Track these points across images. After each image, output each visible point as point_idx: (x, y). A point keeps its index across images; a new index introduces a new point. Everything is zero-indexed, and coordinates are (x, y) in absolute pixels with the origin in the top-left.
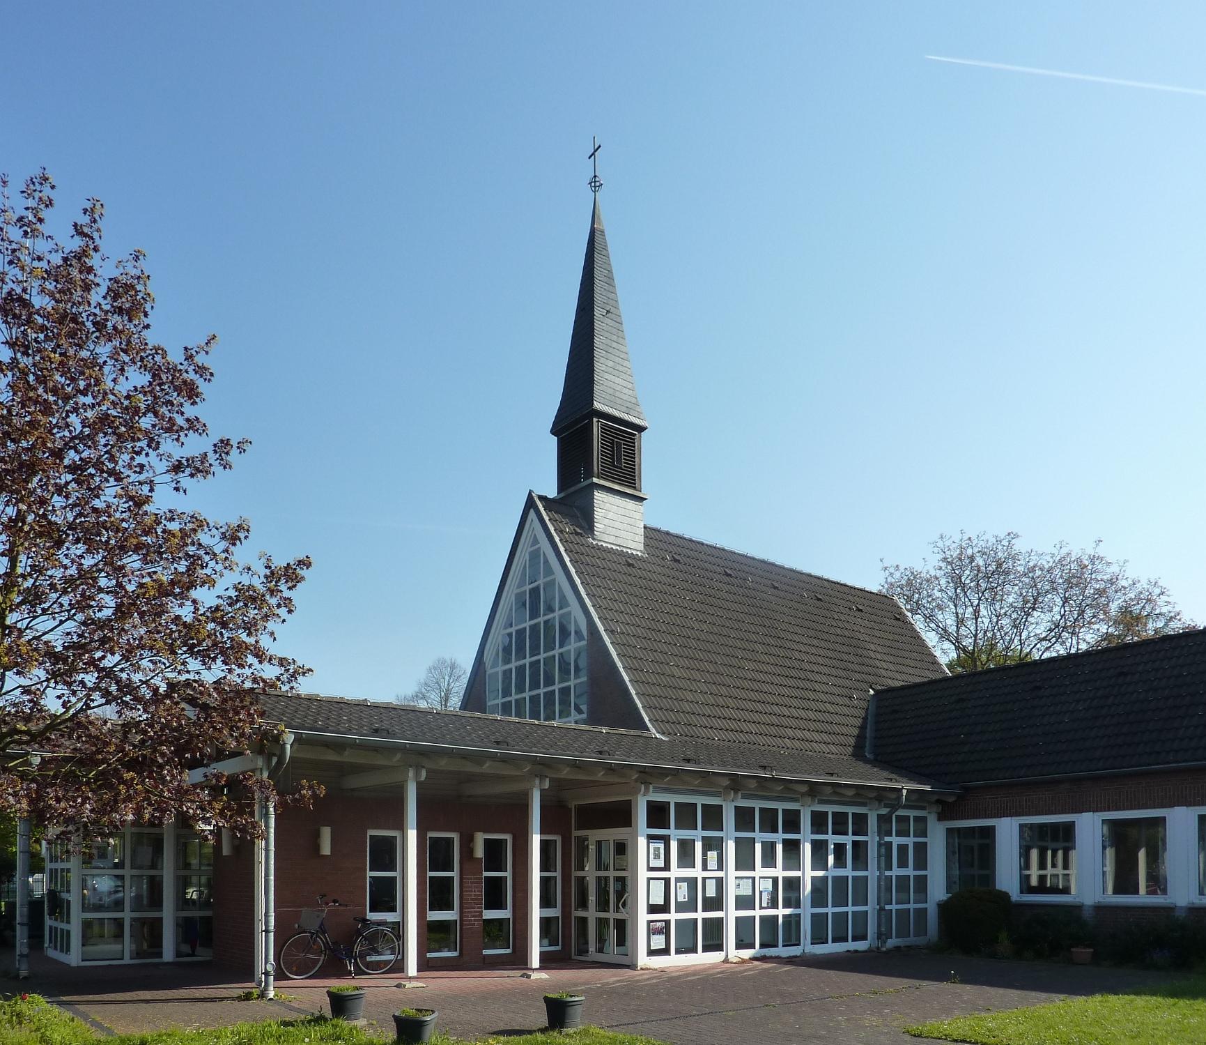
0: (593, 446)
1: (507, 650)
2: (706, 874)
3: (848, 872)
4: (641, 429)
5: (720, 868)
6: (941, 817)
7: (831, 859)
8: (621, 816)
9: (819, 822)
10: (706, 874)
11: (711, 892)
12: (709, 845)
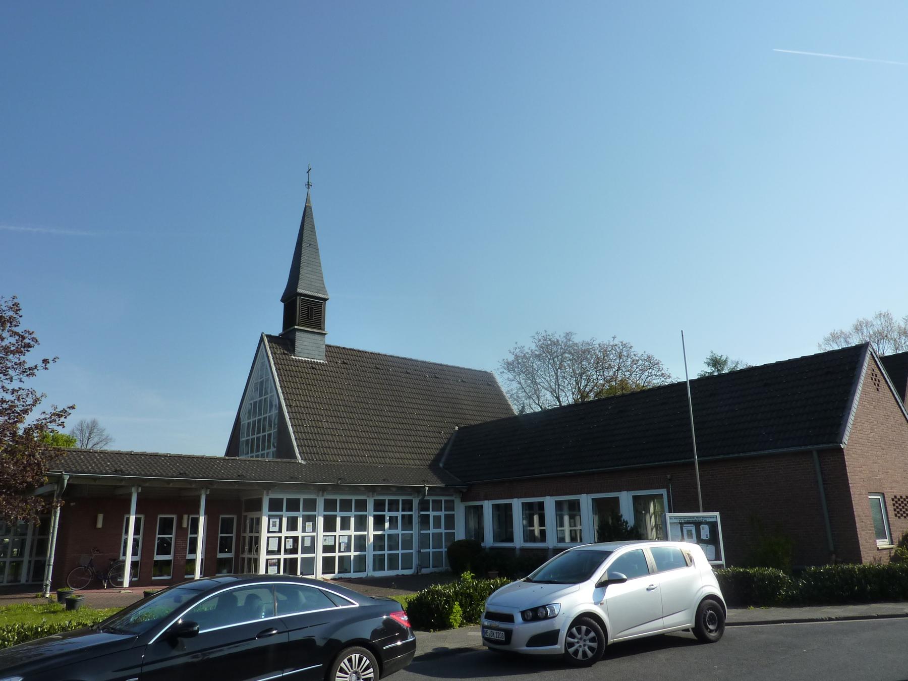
0: (303, 310)
1: (249, 412)
2: (304, 534)
3: (399, 531)
4: (325, 300)
5: (314, 531)
6: (463, 500)
7: (387, 525)
8: (256, 506)
9: (379, 506)
10: (304, 534)
11: (308, 543)
12: (307, 519)
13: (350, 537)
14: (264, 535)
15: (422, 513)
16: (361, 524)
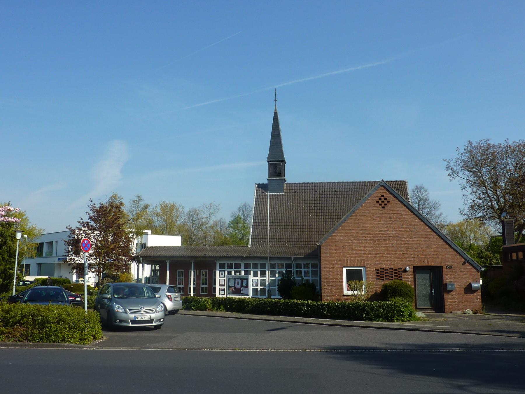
0: (276, 166)
13: (258, 280)
14: (218, 278)
15: (44, 255)
16: (263, 274)
